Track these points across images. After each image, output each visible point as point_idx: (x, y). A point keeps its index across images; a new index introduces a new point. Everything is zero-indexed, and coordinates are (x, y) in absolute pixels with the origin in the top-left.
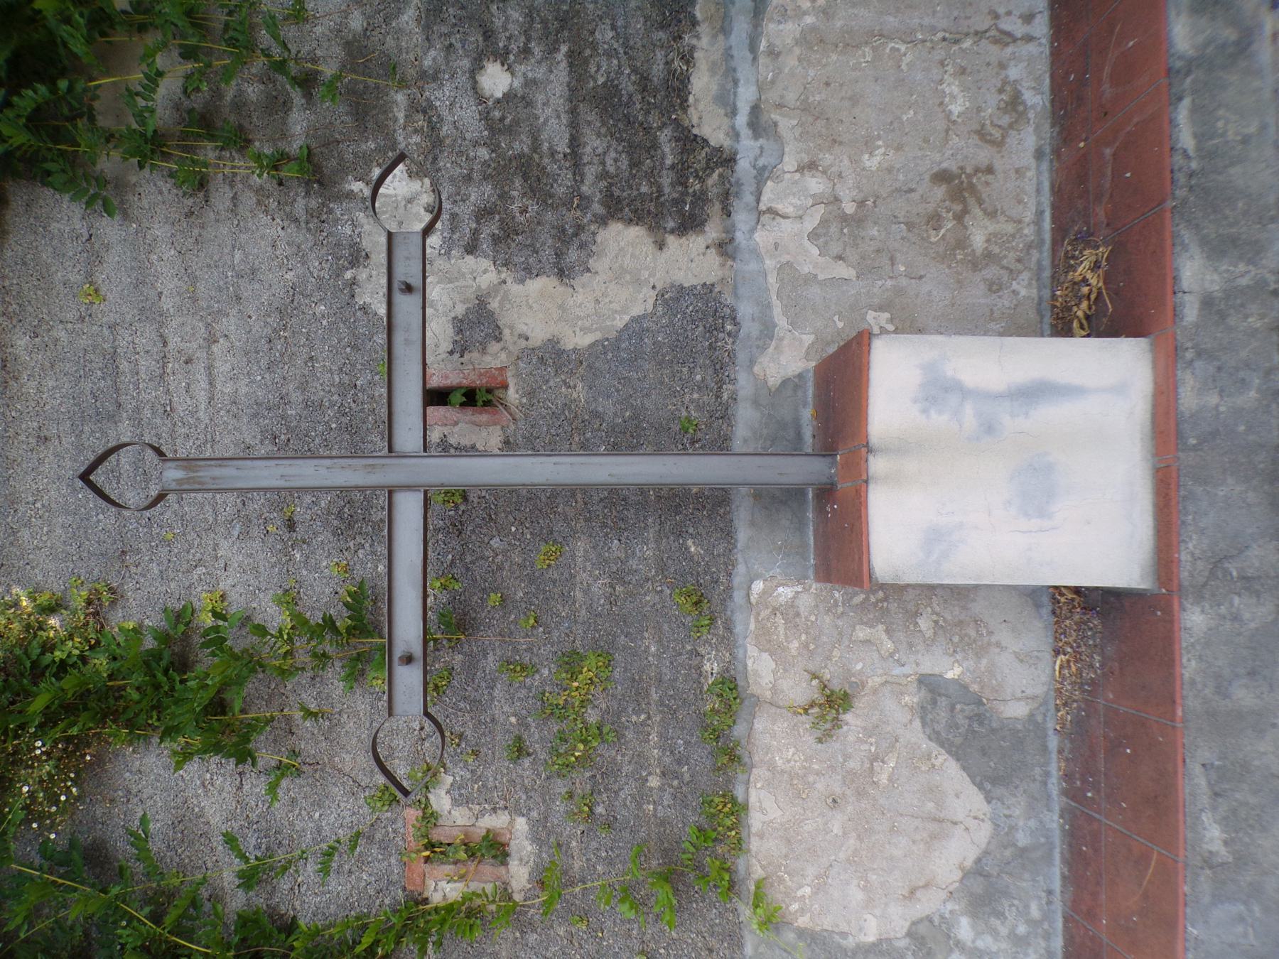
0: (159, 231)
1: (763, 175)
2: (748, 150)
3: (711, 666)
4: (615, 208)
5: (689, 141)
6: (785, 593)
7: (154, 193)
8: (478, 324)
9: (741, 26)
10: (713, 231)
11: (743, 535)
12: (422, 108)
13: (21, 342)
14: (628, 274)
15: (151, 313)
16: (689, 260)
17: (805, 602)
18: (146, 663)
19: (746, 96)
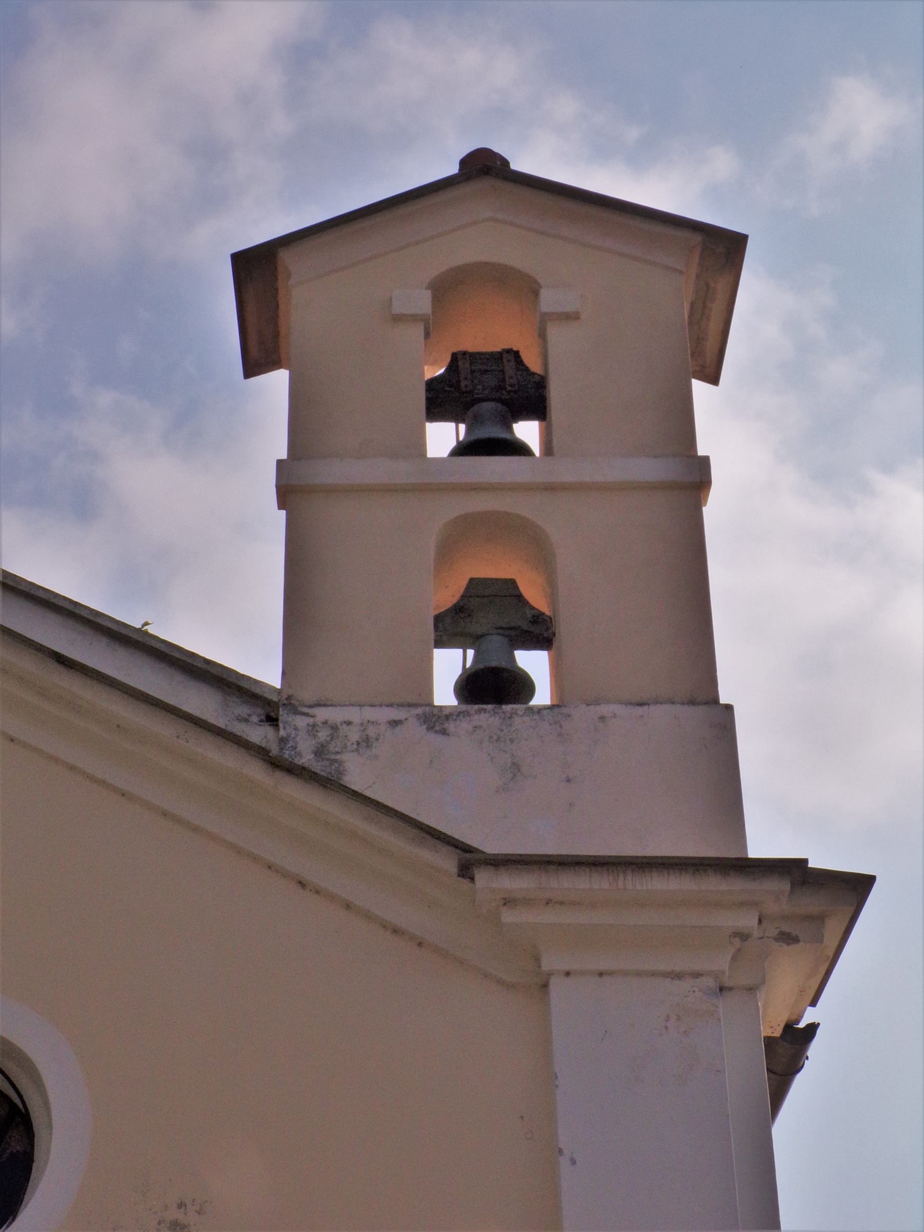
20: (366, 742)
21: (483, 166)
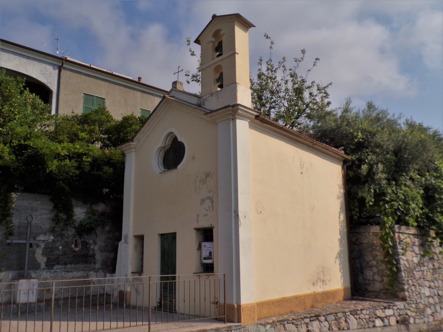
0: (49, 216)
1: (51, 272)
2: (53, 271)
3: (3, 269)
4: (48, 259)
5: (54, 265)
6: (10, 276)
7: (52, 216)
8: (38, 246)
9: (63, 270)
10: (45, 268)
11: (16, 272)
12: (58, 240)
13: (39, 202)
14: (41, 259)
15: (41, 214)
16: (43, 266)
17: (9, 278)
18: (121, 306)
19: (58, 270)
20: (207, 100)
21: (214, 17)
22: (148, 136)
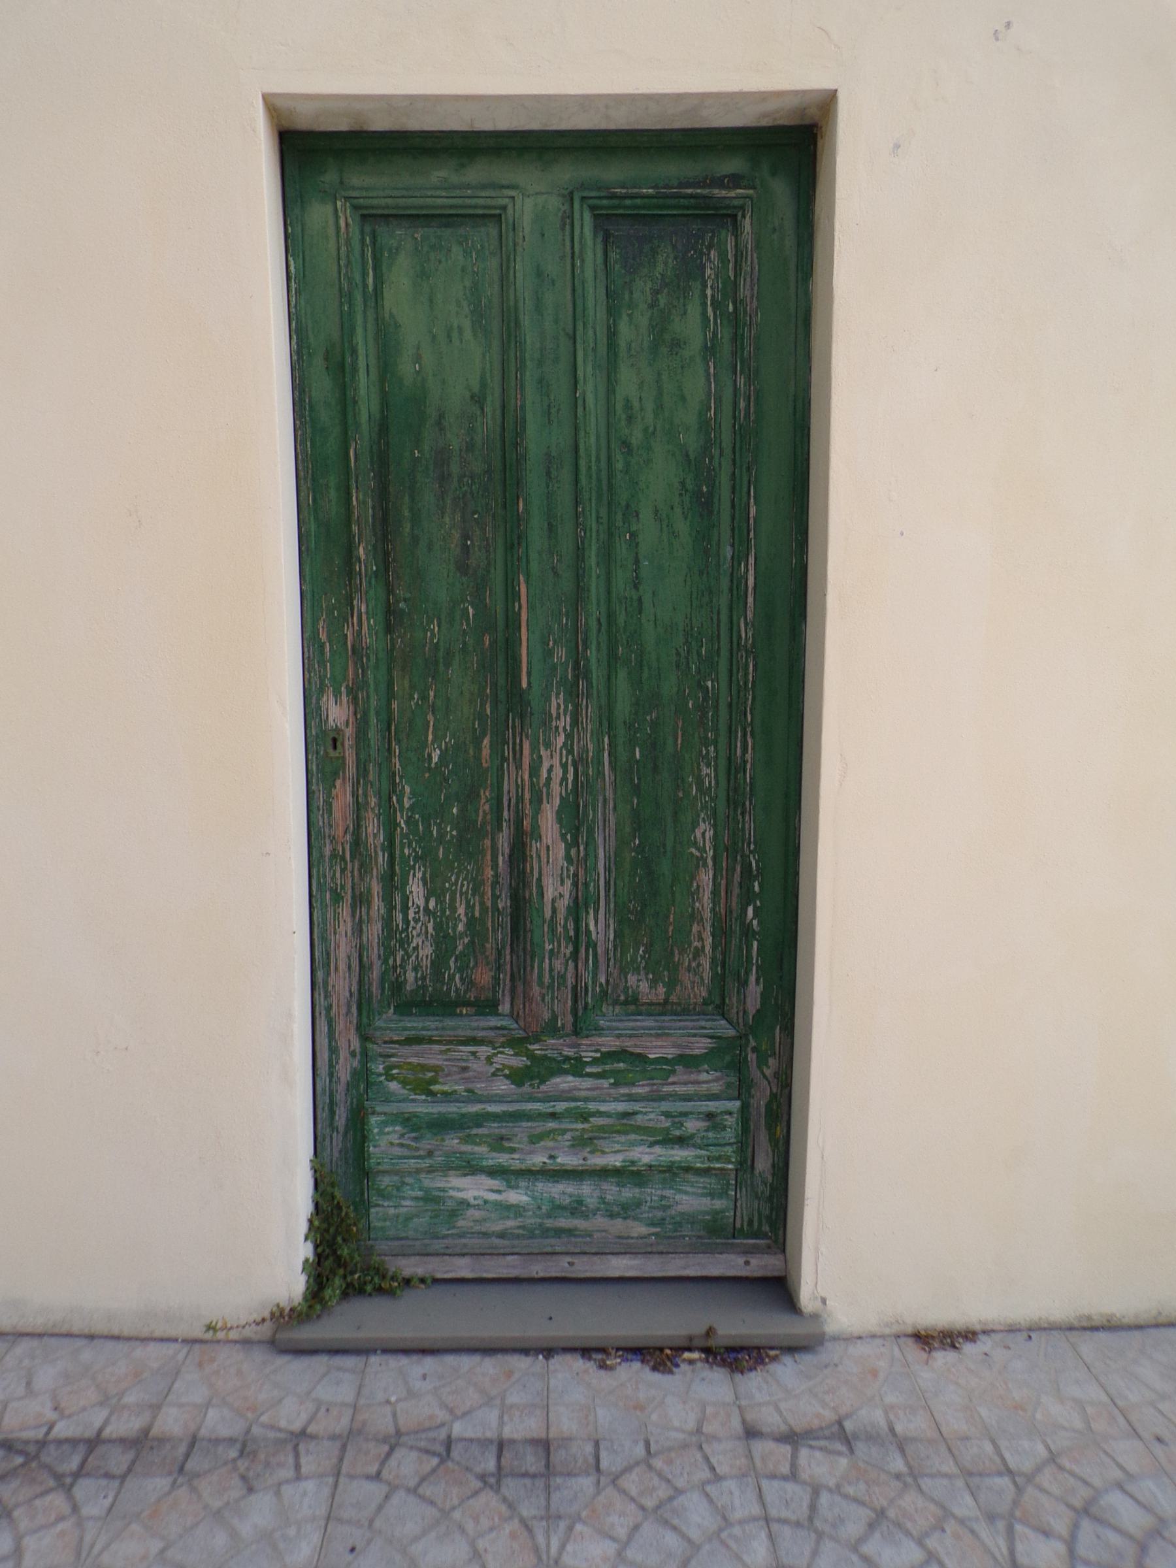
22: (328, 1410)
